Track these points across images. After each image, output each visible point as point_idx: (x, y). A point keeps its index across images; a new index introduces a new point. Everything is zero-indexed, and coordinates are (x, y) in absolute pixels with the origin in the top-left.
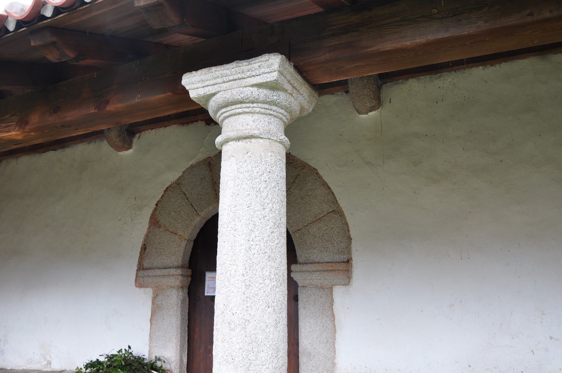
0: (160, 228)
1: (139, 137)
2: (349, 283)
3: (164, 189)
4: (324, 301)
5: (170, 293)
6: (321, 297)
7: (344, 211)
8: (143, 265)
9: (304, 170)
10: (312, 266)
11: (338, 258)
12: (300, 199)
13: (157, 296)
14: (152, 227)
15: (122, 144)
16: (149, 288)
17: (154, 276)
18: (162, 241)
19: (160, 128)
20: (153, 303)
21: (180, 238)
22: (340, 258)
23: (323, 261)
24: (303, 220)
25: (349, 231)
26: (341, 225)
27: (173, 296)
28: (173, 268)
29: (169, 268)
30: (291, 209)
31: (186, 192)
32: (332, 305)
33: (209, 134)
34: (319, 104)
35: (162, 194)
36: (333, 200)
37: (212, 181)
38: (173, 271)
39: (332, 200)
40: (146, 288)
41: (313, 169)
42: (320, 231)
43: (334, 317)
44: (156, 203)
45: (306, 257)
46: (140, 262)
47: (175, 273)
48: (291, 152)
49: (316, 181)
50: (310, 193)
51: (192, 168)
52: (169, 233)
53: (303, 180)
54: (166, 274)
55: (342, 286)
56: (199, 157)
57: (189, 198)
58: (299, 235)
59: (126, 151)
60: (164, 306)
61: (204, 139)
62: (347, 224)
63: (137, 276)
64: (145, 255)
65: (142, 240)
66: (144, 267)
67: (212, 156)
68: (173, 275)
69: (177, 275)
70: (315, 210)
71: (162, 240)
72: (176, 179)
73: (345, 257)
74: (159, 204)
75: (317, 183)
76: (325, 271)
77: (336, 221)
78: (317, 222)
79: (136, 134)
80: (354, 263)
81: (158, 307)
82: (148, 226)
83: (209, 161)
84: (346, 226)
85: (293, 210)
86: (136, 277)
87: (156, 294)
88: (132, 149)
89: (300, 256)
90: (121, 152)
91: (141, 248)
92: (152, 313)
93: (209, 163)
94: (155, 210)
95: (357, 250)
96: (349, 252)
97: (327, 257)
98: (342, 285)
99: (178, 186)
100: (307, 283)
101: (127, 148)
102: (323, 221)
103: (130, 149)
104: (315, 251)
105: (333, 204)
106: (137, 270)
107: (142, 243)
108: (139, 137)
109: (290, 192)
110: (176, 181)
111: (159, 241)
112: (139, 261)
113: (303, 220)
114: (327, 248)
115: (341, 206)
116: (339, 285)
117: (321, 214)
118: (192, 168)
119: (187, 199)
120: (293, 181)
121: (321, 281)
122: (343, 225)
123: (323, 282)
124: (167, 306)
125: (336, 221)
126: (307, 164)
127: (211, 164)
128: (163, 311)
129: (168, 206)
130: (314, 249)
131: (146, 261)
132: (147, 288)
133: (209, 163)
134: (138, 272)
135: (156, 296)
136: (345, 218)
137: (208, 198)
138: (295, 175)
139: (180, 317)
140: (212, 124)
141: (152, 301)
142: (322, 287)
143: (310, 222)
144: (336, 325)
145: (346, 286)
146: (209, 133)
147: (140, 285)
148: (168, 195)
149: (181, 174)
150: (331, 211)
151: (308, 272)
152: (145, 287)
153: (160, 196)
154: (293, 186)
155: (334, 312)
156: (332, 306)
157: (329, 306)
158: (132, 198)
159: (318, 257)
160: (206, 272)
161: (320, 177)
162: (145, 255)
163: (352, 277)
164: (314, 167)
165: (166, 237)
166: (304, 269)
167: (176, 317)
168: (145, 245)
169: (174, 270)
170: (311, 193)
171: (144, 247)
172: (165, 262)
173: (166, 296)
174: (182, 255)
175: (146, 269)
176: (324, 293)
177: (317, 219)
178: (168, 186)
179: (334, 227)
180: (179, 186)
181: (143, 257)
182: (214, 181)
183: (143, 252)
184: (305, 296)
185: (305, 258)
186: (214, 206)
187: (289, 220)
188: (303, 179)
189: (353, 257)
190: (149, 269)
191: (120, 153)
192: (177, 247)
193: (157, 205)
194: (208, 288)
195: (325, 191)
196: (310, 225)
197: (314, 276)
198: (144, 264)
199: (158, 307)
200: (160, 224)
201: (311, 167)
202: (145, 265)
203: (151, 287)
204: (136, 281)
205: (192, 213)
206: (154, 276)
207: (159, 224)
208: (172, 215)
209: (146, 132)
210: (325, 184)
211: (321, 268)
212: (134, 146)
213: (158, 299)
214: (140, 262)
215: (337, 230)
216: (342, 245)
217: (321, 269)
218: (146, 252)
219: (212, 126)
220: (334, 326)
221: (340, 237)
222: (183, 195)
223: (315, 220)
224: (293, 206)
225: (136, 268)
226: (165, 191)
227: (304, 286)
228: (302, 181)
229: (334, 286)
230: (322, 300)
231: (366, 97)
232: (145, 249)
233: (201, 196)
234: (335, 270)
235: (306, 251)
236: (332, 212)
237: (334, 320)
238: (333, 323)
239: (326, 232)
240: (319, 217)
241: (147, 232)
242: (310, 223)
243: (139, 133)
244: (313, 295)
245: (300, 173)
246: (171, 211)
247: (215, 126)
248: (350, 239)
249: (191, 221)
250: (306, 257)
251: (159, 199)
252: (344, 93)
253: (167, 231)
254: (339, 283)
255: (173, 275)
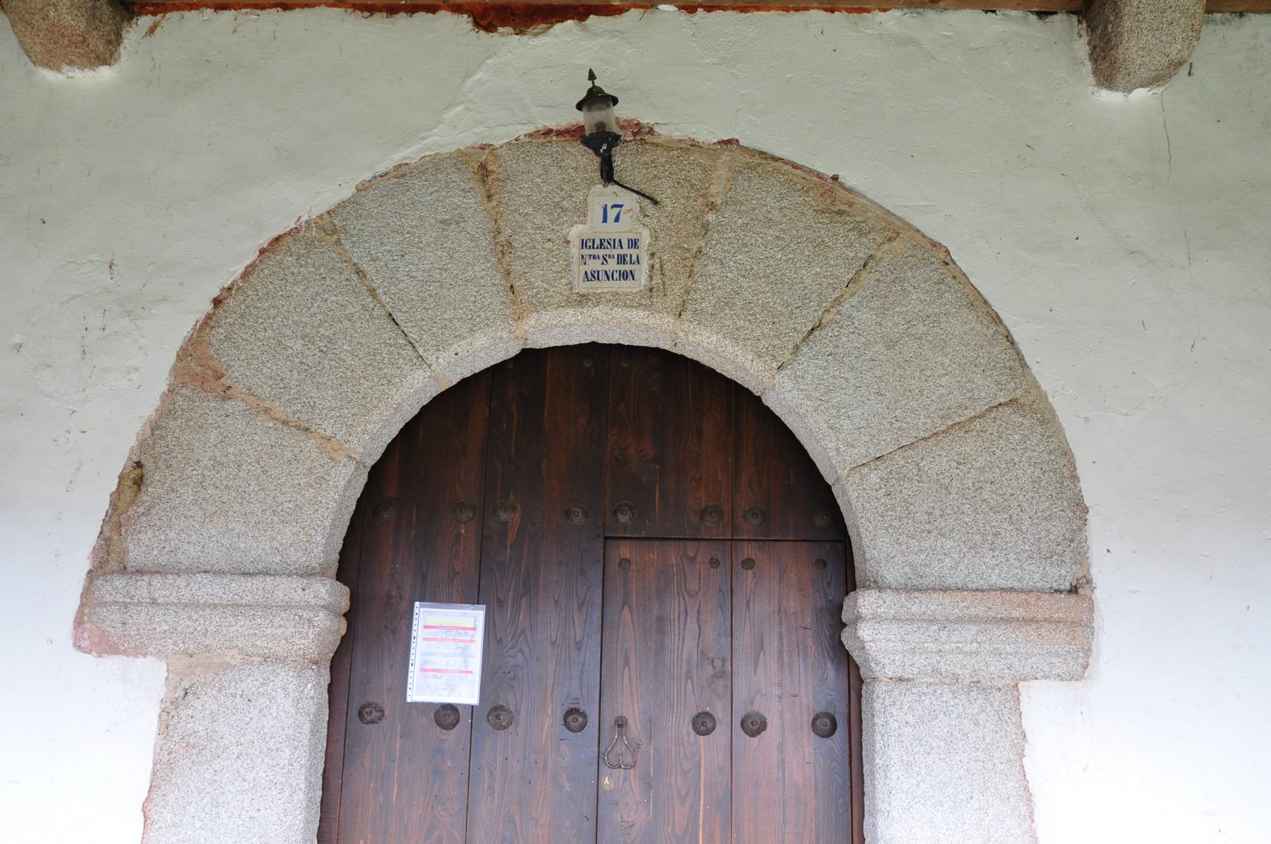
0: (226, 398)
1: (152, 31)
2: (1084, 672)
3: (261, 242)
4: (987, 741)
5: (262, 684)
6: (977, 724)
7: (1055, 407)
8: (125, 552)
9: (894, 244)
10: (947, 599)
11: (1037, 577)
12: (880, 346)
13: (190, 697)
14: (184, 391)
15: (82, 28)
16: (149, 659)
17: (186, 605)
18: (232, 457)
19: (258, 11)
20: (165, 729)
21: (329, 448)
22: (1044, 575)
23: (982, 582)
24: (898, 425)
25: (1075, 478)
26: (1045, 455)
27: (272, 699)
28: (289, 575)
29: (265, 573)
30: (846, 379)
31: (365, 267)
32: (1021, 755)
33: (489, 62)
34: (944, 35)
35: (247, 262)
36: (1011, 363)
37: (494, 237)
38: (287, 589)
39: (1008, 364)
40: (130, 659)
41: (929, 246)
42: (965, 469)
43: (1028, 798)
44: (215, 293)
45: (911, 565)
46: (110, 539)
47: (297, 596)
48: (841, 174)
49: (942, 286)
50: (921, 328)
51: (403, 176)
52: (271, 424)
53: (893, 277)
54: (248, 599)
55: (1058, 683)
56: (436, 138)
57: (380, 291)
58: (882, 479)
59: (82, 67)
60: (226, 741)
61: (467, 76)
62: (1067, 454)
63: (88, 597)
64: (141, 510)
65: (133, 442)
66: (129, 566)
67: (496, 144)
68: (286, 607)
69: (308, 606)
70: (943, 391)
71: (231, 450)
72: (322, 209)
73: (1063, 572)
74: (231, 302)
75: (946, 295)
76: (998, 621)
77: (1025, 438)
78: (951, 437)
79: (140, 14)
80: (1099, 595)
81: (188, 744)
82: (165, 388)
83: (482, 160)
84: (1063, 461)
85: (853, 381)
86: (82, 606)
87: (186, 684)
88: (116, 68)
89: (887, 561)
90: (59, 71)
91: (121, 478)
92: (154, 773)
93: (483, 167)
94: (207, 322)
95: (1108, 551)
96: (1081, 558)
97: (997, 571)
98: (1060, 677)
99: (327, 238)
100: (917, 665)
101: (98, 57)
102: (975, 433)
103: (105, 62)
104: (950, 544)
105: (1012, 378)
106: (90, 572)
107: (130, 459)
108: (152, 31)
109: (839, 313)
110: (321, 217)
111: (218, 454)
112: (101, 532)
113: (898, 425)
114: (996, 534)
115: (1045, 386)
116: (1047, 677)
117: (966, 409)
118: (403, 176)
119: (372, 292)
120: (849, 277)
121: (973, 661)
122: (1053, 457)
123: (982, 664)
124: (239, 744)
125: (1025, 438)
126: (908, 224)
127: (492, 172)
128: (217, 767)
129: (273, 312)
130: (943, 535)
131: (142, 536)
132: (136, 656)
133: (483, 167)
134: (98, 582)
135: (182, 694)
136: (1059, 431)
137: (473, 299)
138: (860, 255)
139: (302, 796)
140: (501, 29)
141: (160, 715)
142: (979, 682)
143: (922, 434)
144: (1040, 834)
145: (1073, 682)
146: (489, 57)
147: (100, 643)
148: (275, 269)
149: (347, 192)
150: (1002, 401)
151: (933, 621)
152: (125, 653)
153: (240, 269)
154: (852, 296)
155: (1030, 785)
156: (1021, 760)
157: (1009, 761)
158: (91, 262)
159: (962, 567)
160: (417, 604)
161: (960, 277)
162: (141, 510)
163: (1094, 647)
164: (936, 238)
165: (257, 438)
166: (915, 609)
167: (287, 793)
168: (139, 465)
169: (297, 583)
170: (924, 329)
171: (132, 476)
172: (242, 545)
173: (238, 700)
174: (327, 523)
175: (140, 572)
176: (989, 708)
177: (952, 426)
178: (281, 233)
179: (1017, 460)
180: (335, 237)
181: (129, 518)
182: (502, 239)
183: (128, 493)
184: (910, 719)
185: (907, 569)
186: (499, 334)
187: (839, 417)
188: (892, 273)
189: (1095, 572)
190: (161, 571)
191: (48, 75)
192: (311, 486)
193: (217, 302)
194: (423, 670)
195: (979, 327)
196: (923, 443)
197: (954, 639)
198: (131, 547)
199: (188, 744)
200: (229, 382)
201: (924, 236)
202: (136, 554)
203: (159, 654)
204: (79, 622)
205: (391, 353)
206: (186, 605)
207: (223, 381)
208: (290, 351)
209: (186, 14)
210: (978, 303)
211: (980, 610)
212: (123, 59)
213: (190, 712)
214: (110, 539)
215: (1029, 471)
216: (1053, 529)
217: (981, 614)
218: (145, 498)
219: (502, 35)
220: (1031, 836)
221: (1043, 499)
222: (354, 277)
223: (944, 428)
224: (852, 369)
225: (86, 565)
226: (262, 252)
227: (900, 680)
228: (888, 280)
229: (1024, 680)
230: (980, 734)
231: (1183, 19)
232: (139, 482)
233: (441, 286)
234: (1033, 620)
235: (911, 541)
236: (1006, 404)
237: (1032, 813)
238: (1026, 826)
239: (989, 476)
240: (957, 420)
241: (157, 410)
242: (925, 439)
243: (154, 14)
244: (941, 716)
245: (879, 255)
246: (289, 332)
247: (518, 37)
248: (1080, 508)
249: (385, 382)
250: (911, 565)
251: (231, 280)
252: (1033, 18)
253: (262, 417)
254: (1046, 668)
255: (286, 607)
